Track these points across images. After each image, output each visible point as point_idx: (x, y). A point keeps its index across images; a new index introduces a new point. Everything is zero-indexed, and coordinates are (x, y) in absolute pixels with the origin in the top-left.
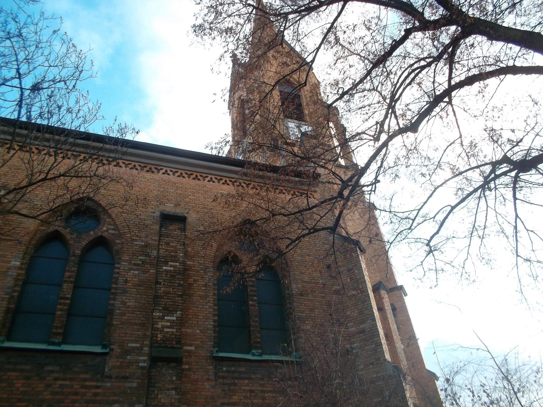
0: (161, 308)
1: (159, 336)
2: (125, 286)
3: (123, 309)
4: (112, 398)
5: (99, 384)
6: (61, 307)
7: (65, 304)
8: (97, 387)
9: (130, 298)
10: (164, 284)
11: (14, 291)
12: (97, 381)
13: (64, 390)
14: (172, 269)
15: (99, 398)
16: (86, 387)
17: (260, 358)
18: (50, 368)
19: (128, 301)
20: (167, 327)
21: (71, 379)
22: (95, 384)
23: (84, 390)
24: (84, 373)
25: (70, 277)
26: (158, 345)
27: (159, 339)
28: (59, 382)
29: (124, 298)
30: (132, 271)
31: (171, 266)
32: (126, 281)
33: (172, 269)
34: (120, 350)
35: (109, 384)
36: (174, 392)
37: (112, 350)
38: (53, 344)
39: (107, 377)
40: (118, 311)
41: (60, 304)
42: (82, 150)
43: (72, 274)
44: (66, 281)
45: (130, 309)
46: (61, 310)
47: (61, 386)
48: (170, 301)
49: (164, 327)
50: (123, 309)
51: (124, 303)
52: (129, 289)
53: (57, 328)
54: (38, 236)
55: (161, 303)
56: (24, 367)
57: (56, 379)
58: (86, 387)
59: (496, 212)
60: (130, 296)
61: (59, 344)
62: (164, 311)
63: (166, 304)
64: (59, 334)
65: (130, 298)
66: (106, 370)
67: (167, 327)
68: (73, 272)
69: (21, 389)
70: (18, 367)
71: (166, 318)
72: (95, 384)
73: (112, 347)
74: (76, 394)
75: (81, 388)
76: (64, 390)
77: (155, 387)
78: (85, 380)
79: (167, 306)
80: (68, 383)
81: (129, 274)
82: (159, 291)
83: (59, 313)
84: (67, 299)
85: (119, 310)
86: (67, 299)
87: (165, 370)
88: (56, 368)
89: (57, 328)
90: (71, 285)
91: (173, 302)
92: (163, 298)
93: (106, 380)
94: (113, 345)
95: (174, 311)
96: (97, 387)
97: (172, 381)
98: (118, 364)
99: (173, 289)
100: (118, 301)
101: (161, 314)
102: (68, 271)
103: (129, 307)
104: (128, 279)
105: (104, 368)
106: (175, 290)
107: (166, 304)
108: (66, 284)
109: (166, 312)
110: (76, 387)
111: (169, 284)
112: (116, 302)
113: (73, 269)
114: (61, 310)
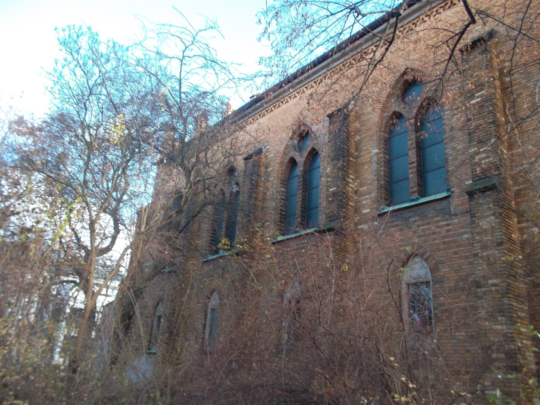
0: (475, 143)
1: (478, 169)
2: (452, 133)
3: (455, 154)
4: (460, 231)
5: (449, 222)
6: (411, 171)
7: (413, 168)
8: (448, 225)
9: (459, 142)
10: (474, 119)
11: (381, 171)
12: (447, 220)
13: (426, 233)
14: (479, 99)
15: (451, 233)
16: (439, 227)
17: (416, 203)
18: (413, 219)
19: (457, 145)
20: (484, 158)
21: (428, 224)
22: (445, 223)
23: (439, 230)
24: (437, 216)
25: (411, 145)
26: (478, 178)
27: (478, 172)
28: (421, 228)
29: (453, 144)
30: (455, 117)
31: (478, 97)
32: (452, 129)
33: (479, 99)
34: (459, 191)
35: (456, 221)
36: (493, 218)
37: (452, 192)
38: (413, 200)
39: (453, 215)
40: (450, 158)
41: (410, 169)
42: (324, 71)
43: (413, 141)
44: (409, 149)
45: (460, 152)
46: (412, 173)
47: (423, 230)
48: (483, 132)
49: (480, 160)
50: (455, 154)
51: (454, 149)
52: (455, 135)
53: (412, 188)
54: (384, 122)
55: (475, 138)
56: (397, 223)
57: (418, 226)
58: (439, 227)
59: (354, 23)
60: (458, 140)
61: (417, 199)
62: (478, 145)
63: (479, 137)
64: (415, 192)
65: (459, 142)
66: (452, 210)
67: (484, 158)
68: (412, 139)
69: (399, 238)
70: (394, 224)
71: (481, 150)
72: (445, 223)
73: (453, 189)
74: (434, 233)
75: (437, 228)
76: (426, 233)
77: (475, 217)
78: (438, 222)
79: (480, 139)
80: (426, 227)
81: (453, 120)
82: (471, 128)
83: (411, 176)
84: (414, 163)
85: (451, 156)
86: (414, 163)
87: (482, 200)
88: (417, 218)
89: (412, 188)
90: (414, 151)
91: (485, 132)
92: (476, 133)
93: (453, 217)
94: (453, 187)
95: (487, 140)
96: (448, 225)
97: (490, 207)
98: (460, 202)
99: (483, 119)
100: (449, 149)
101: (476, 149)
102: (409, 141)
103: (459, 150)
104: (453, 125)
105: (450, 209)
106: (485, 120)
107: (479, 137)
108: (410, 152)
109: (480, 144)
110: (433, 228)
111: (479, 116)
112: (448, 151)
113: (412, 136)
114: (412, 173)
